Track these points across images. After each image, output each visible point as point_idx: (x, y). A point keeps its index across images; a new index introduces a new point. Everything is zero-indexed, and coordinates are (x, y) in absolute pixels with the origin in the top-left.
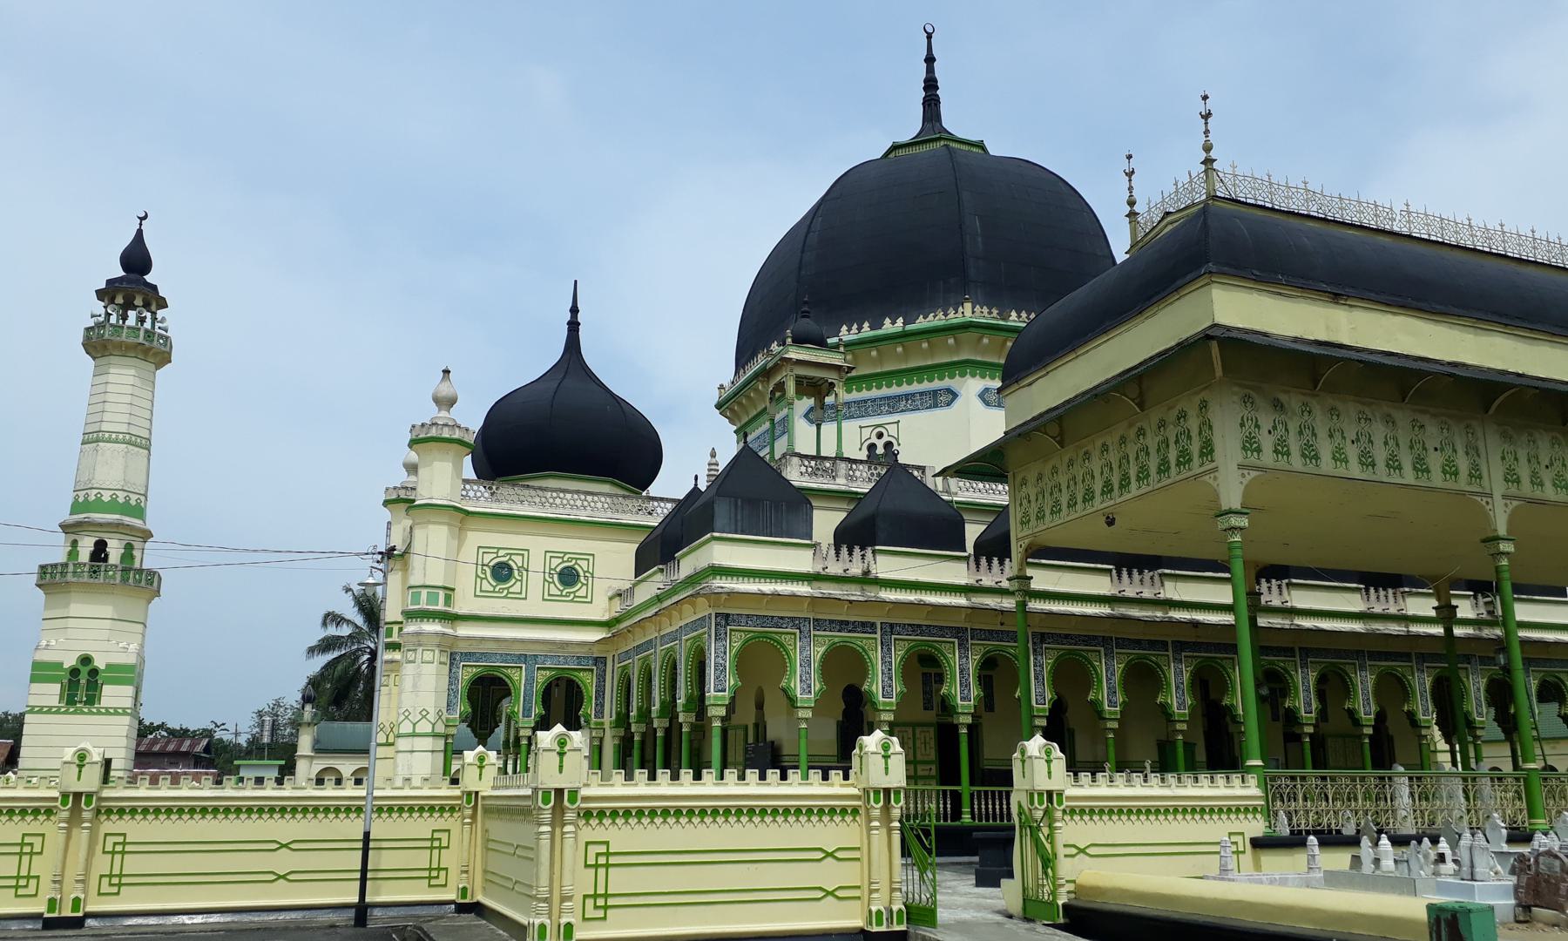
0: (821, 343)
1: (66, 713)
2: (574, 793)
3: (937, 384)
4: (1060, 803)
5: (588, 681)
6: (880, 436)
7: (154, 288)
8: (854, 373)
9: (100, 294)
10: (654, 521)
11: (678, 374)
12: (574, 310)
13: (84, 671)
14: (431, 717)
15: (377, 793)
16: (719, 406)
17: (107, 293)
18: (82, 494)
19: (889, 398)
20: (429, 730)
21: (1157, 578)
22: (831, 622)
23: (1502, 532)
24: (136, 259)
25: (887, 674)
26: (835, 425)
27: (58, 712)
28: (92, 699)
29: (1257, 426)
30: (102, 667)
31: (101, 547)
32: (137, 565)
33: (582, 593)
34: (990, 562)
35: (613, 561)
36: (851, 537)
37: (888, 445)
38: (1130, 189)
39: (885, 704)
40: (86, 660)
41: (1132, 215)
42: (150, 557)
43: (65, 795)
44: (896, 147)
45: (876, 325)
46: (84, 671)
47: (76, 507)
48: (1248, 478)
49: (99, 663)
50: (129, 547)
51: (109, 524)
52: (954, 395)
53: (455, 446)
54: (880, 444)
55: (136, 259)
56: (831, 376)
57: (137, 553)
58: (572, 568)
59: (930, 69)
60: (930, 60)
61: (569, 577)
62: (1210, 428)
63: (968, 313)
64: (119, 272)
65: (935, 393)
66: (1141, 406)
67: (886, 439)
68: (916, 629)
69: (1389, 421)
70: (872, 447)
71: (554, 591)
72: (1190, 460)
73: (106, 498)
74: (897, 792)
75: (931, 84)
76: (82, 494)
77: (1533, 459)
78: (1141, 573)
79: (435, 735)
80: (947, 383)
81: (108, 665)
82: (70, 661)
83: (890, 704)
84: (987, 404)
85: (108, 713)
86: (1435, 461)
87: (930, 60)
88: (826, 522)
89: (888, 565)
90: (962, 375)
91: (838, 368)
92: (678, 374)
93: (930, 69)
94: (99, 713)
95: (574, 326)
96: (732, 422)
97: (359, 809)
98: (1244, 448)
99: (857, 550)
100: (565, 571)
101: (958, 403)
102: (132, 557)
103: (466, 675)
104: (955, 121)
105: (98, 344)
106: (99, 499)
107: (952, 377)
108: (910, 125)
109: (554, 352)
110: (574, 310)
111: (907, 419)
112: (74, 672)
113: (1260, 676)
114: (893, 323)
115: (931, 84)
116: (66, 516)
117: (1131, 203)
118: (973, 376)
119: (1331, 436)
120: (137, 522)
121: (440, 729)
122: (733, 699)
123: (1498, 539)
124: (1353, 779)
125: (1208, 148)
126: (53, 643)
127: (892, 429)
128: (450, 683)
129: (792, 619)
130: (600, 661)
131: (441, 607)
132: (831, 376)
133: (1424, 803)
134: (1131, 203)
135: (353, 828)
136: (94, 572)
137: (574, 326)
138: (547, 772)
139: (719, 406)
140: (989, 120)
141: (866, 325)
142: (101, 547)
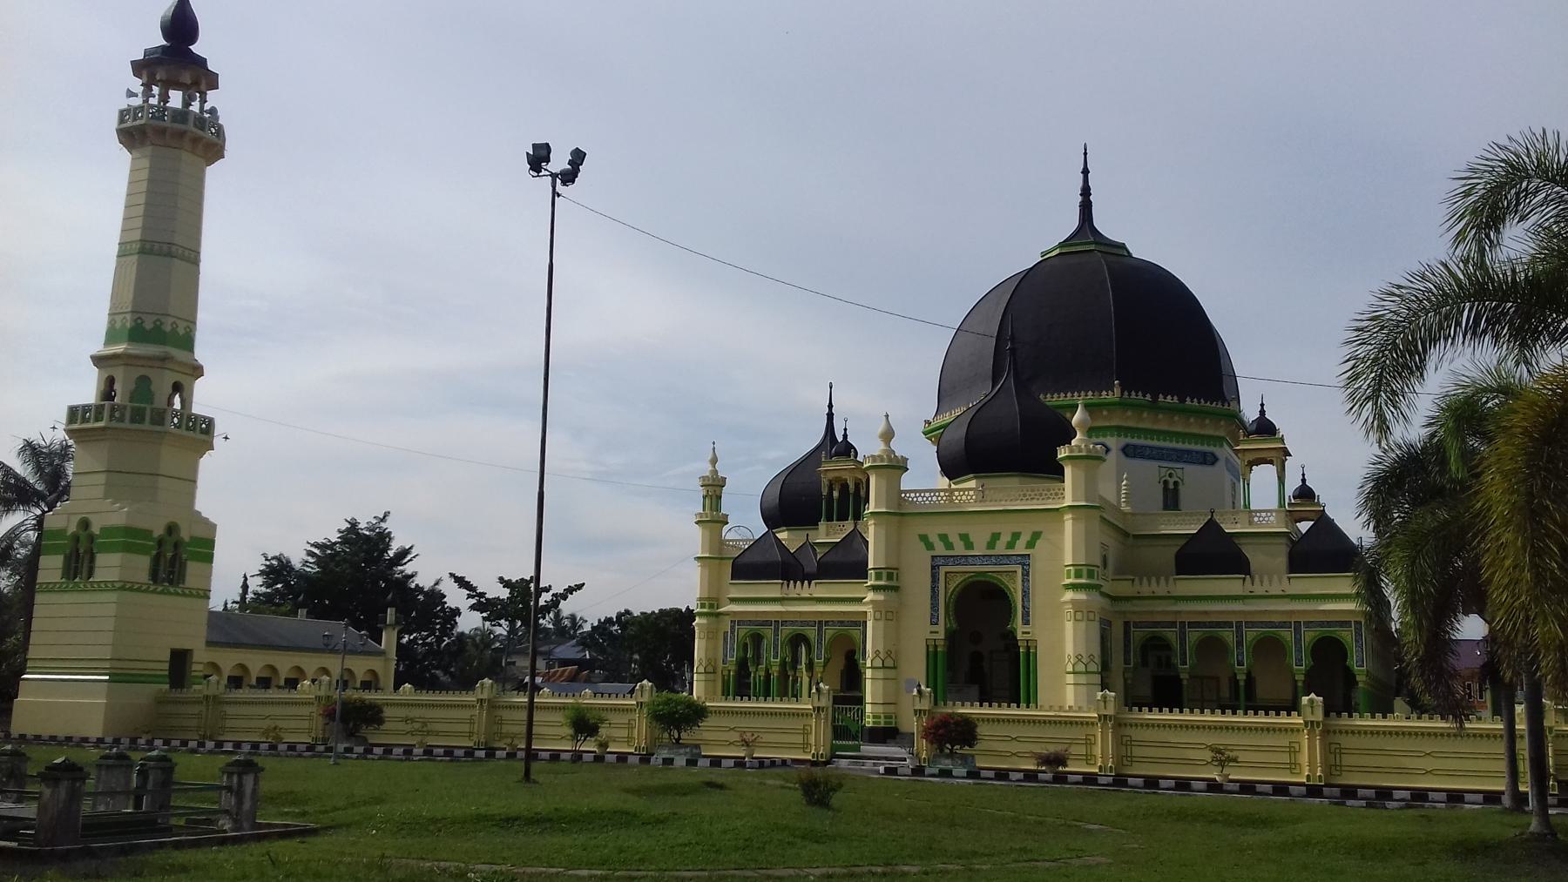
1: (154, 592)
9: (138, 68)
17: (146, 67)
27: (145, 591)
30: (187, 539)
37: (1176, 483)
40: (171, 529)
43: (1306, 723)
45: (1182, 400)
49: (185, 535)
51: (149, 358)
54: (1171, 481)
60: (1086, 172)
64: (159, 41)
70: (1166, 482)
75: (1086, 191)
82: (159, 531)
85: (191, 595)
87: (1086, 172)
94: (184, 595)
111: (1189, 468)
113: (192, 568)
115: (1086, 191)
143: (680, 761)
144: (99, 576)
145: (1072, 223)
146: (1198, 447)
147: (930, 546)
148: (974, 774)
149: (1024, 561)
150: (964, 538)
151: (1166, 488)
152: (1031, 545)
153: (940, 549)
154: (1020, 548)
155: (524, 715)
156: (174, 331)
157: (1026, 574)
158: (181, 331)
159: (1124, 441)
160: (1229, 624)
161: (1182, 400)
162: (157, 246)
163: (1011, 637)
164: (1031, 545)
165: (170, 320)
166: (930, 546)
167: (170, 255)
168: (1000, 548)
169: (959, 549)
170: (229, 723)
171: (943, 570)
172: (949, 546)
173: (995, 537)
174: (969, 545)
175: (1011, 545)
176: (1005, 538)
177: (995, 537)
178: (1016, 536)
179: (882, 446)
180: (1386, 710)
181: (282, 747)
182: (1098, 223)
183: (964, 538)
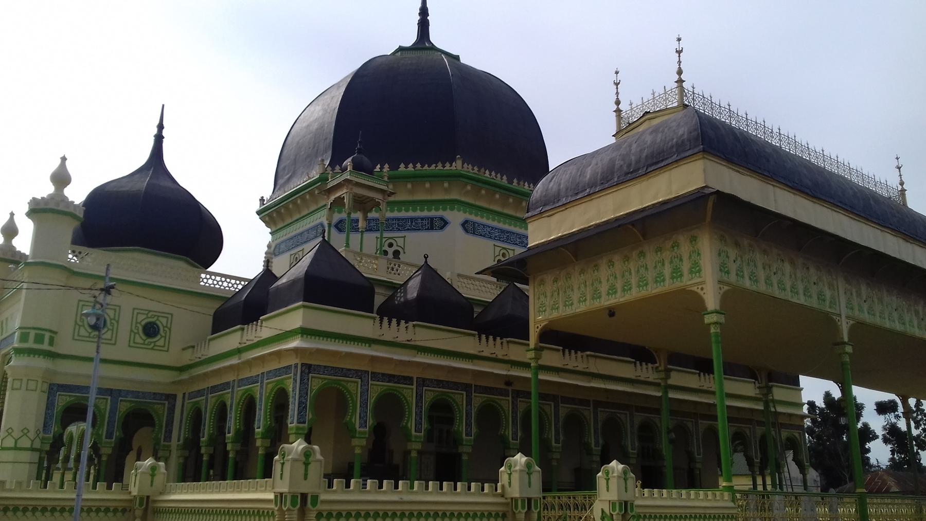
0: (370, 172)
2: (315, 498)
3: (433, 213)
4: (632, 510)
6: (391, 245)
8: (392, 199)
12: (161, 127)
14: (32, 435)
15: (84, 496)
16: (259, 213)
19: (398, 219)
20: (28, 445)
21: (585, 357)
22: (383, 375)
23: (846, 339)
25: (418, 414)
26: (359, 235)
29: (728, 257)
33: (161, 343)
34: (487, 339)
38: (617, 93)
39: (416, 437)
41: (618, 111)
48: (723, 290)
53: (50, 215)
56: (378, 197)
58: (154, 323)
61: (151, 330)
62: (699, 254)
63: (459, 167)
65: (432, 219)
66: (644, 235)
67: (395, 248)
68: (439, 383)
69: (792, 263)
71: (138, 340)
72: (682, 275)
74: (536, 501)
77: (859, 295)
78: (576, 353)
79: (33, 449)
80: (440, 213)
83: (420, 437)
84: (466, 231)
86: (814, 290)
90: (452, 209)
91: (382, 191)
95: (159, 139)
96: (268, 225)
97: (71, 510)
98: (721, 270)
99: (403, 322)
101: (448, 229)
104: (437, 38)
107: (444, 209)
108: (409, 38)
109: (142, 157)
110: (161, 127)
114: (406, 167)
117: (618, 102)
118: (459, 211)
119: (764, 268)
121: (37, 444)
122: (310, 430)
123: (845, 343)
124: (554, 497)
125: (680, 72)
127: (400, 242)
128: (47, 408)
129: (357, 371)
130: (171, 398)
131: (45, 346)
132: (378, 197)
133: (546, 511)
134: (618, 102)
137: (159, 139)
139: (259, 213)
140: (466, 40)
141: (386, 166)
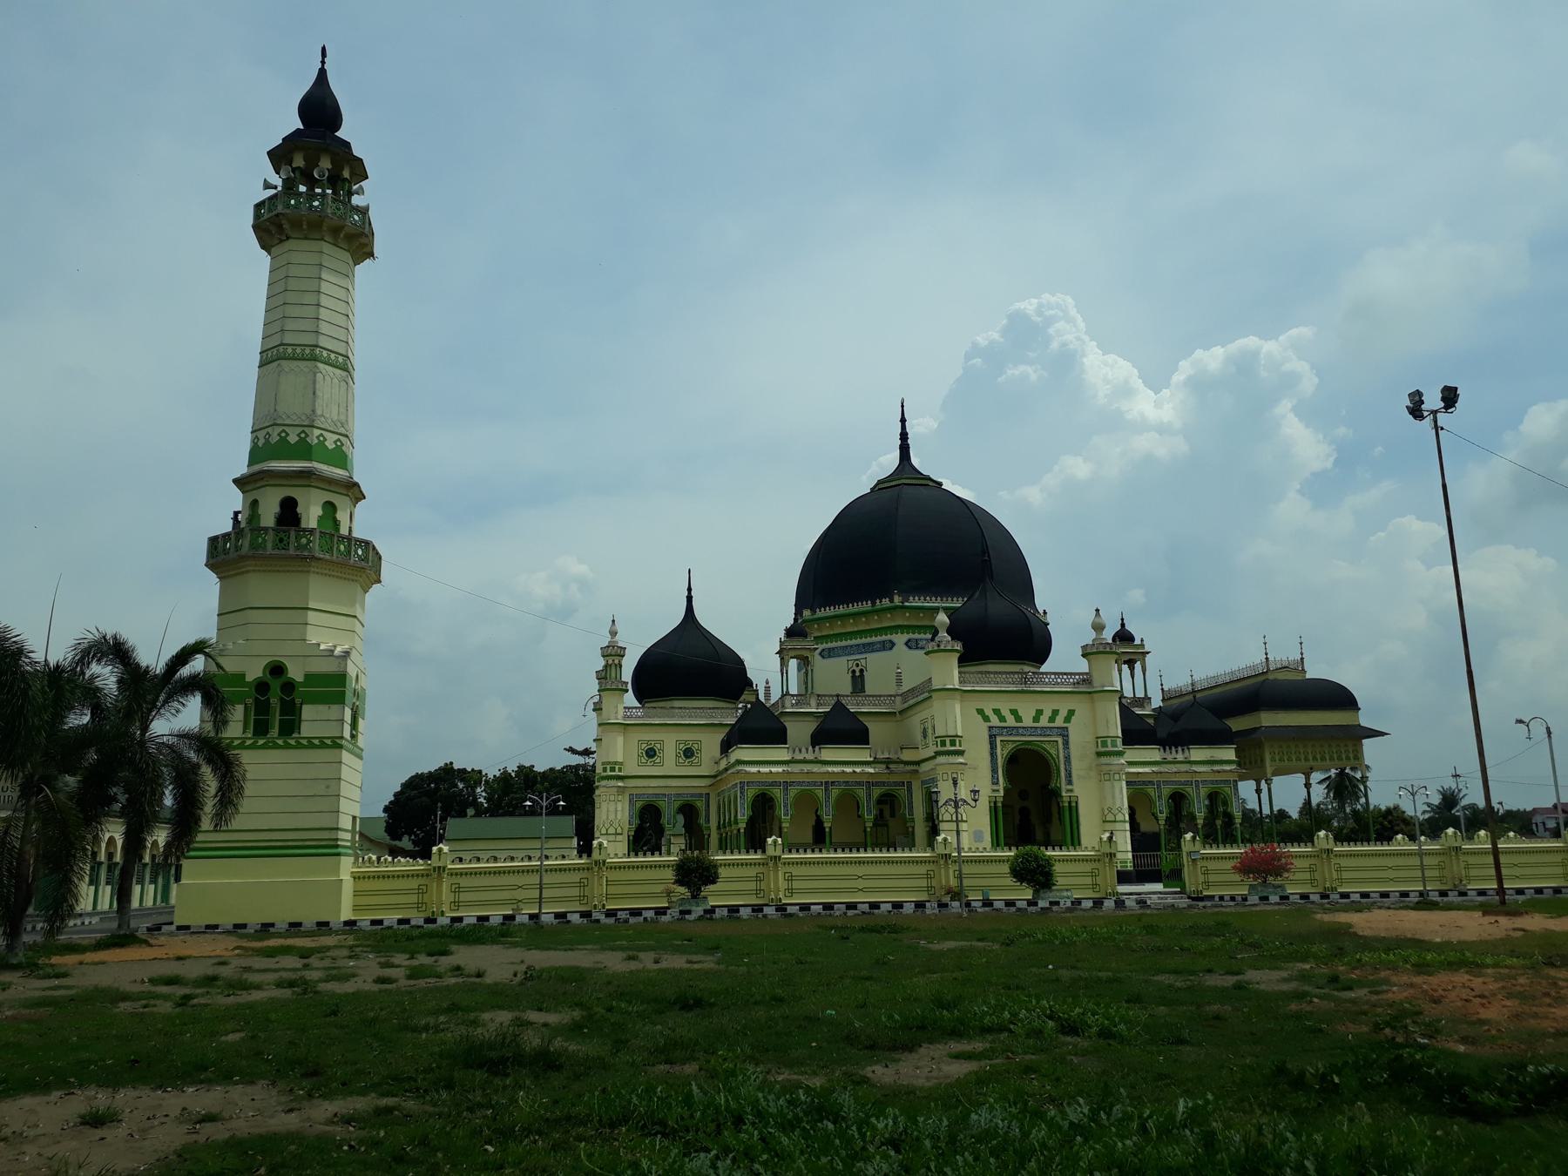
1: (253, 747)
5: (700, 805)
7: (347, 145)
10: (733, 722)
11: (754, 622)
12: (689, 589)
13: (275, 685)
18: (261, 434)
24: (320, 110)
28: (290, 726)
31: (289, 506)
32: (344, 531)
35: (710, 744)
36: (819, 739)
40: (277, 669)
42: (362, 522)
44: (880, 482)
46: (275, 685)
47: (255, 455)
49: (295, 673)
50: (330, 507)
52: (893, 644)
55: (320, 110)
57: (342, 516)
59: (903, 427)
60: (903, 421)
73: (293, 439)
75: (904, 436)
76: (261, 434)
80: (889, 637)
81: (307, 676)
82: (255, 672)
85: (311, 746)
87: (903, 421)
88: (799, 732)
89: (828, 753)
92: (754, 622)
93: (903, 427)
94: (299, 746)
95: (689, 598)
100: (680, 749)
102: (336, 524)
103: (639, 805)
105: (272, 226)
106: (283, 440)
110: (689, 589)
112: (261, 687)
115: (904, 436)
116: (242, 469)
120: (339, 472)
126: (230, 646)
135: (535, 879)
136: (281, 543)
137: (689, 598)
138: (770, 851)
142: (289, 506)
143: (1274, 899)
144: (307, 730)
145: (892, 460)
146: (879, 638)
147: (986, 719)
148: (1285, 898)
149: (1064, 733)
150: (1014, 712)
151: (854, 676)
152: (1068, 719)
153: (995, 721)
154: (1059, 722)
155: (1491, 859)
156: (322, 443)
157: (1066, 744)
158: (330, 445)
159: (906, 637)
160: (1151, 783)
161: (874, 604)
162: (298, 350)
163: (1056, 793)
164: (1068, 719)
165: (317, 432)
166: (986, 719)
167: (314, 359)
168: (1044, 722)
169: (1011, 721)
170: (1560, 870)
171: (998, 739)
172: (1002, 719)
173: (1039, 712)
174: (1018, 719)
175: (1052, 719)
176: (1047, 713)
177: (1039, 712)
178: (1055, 712)
179: (1093, 634)
180: (1389, 839)
181: (1334, 897)
182: (915, 461)
183: (1014, 712)
